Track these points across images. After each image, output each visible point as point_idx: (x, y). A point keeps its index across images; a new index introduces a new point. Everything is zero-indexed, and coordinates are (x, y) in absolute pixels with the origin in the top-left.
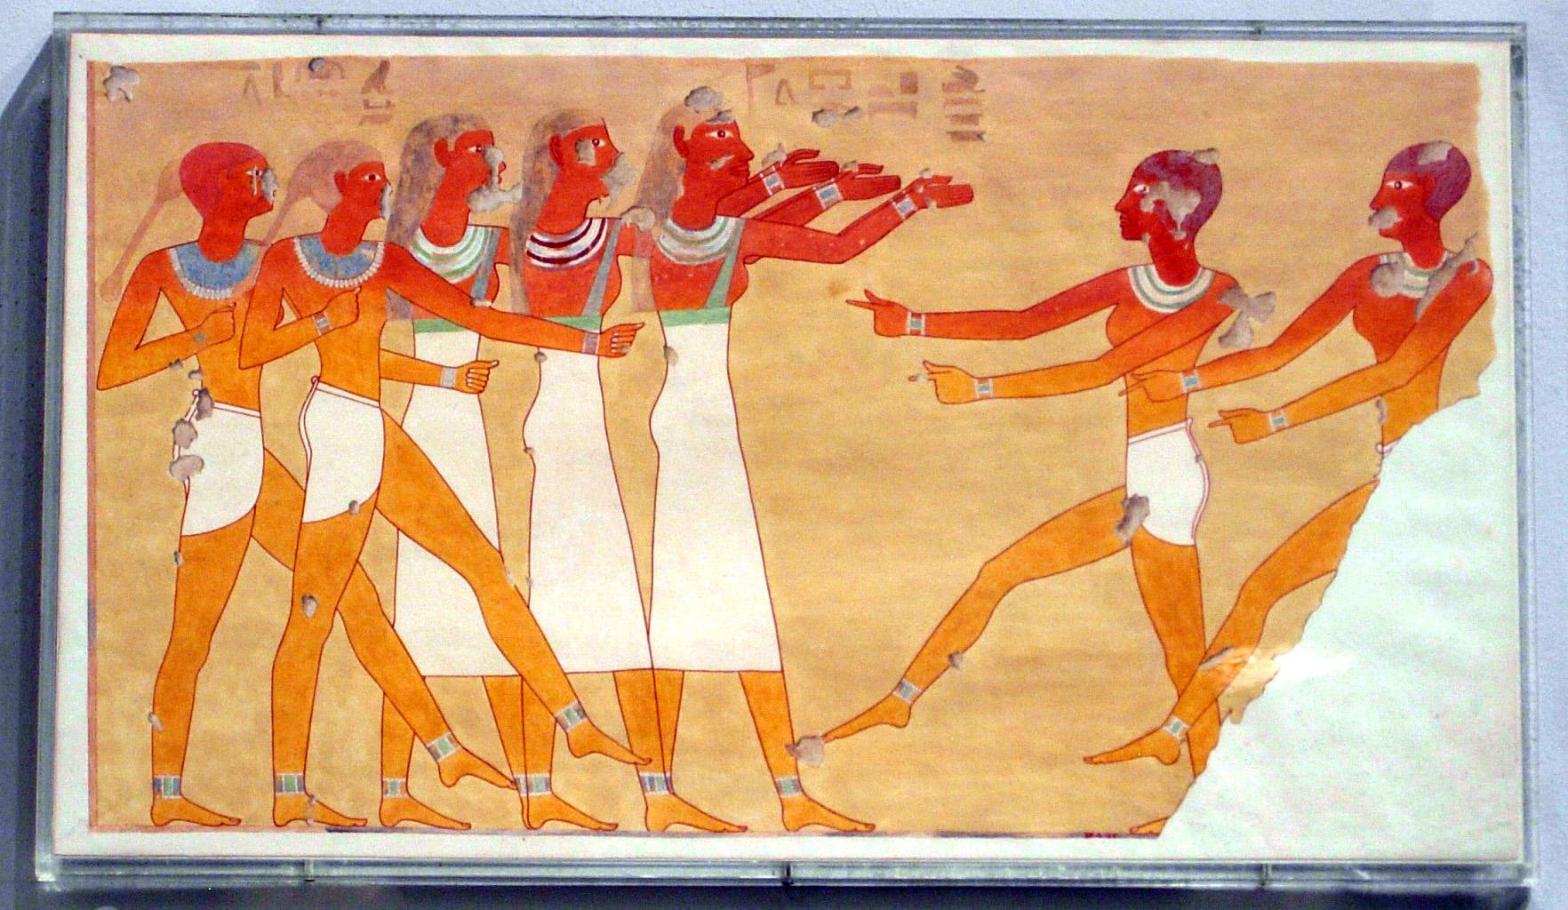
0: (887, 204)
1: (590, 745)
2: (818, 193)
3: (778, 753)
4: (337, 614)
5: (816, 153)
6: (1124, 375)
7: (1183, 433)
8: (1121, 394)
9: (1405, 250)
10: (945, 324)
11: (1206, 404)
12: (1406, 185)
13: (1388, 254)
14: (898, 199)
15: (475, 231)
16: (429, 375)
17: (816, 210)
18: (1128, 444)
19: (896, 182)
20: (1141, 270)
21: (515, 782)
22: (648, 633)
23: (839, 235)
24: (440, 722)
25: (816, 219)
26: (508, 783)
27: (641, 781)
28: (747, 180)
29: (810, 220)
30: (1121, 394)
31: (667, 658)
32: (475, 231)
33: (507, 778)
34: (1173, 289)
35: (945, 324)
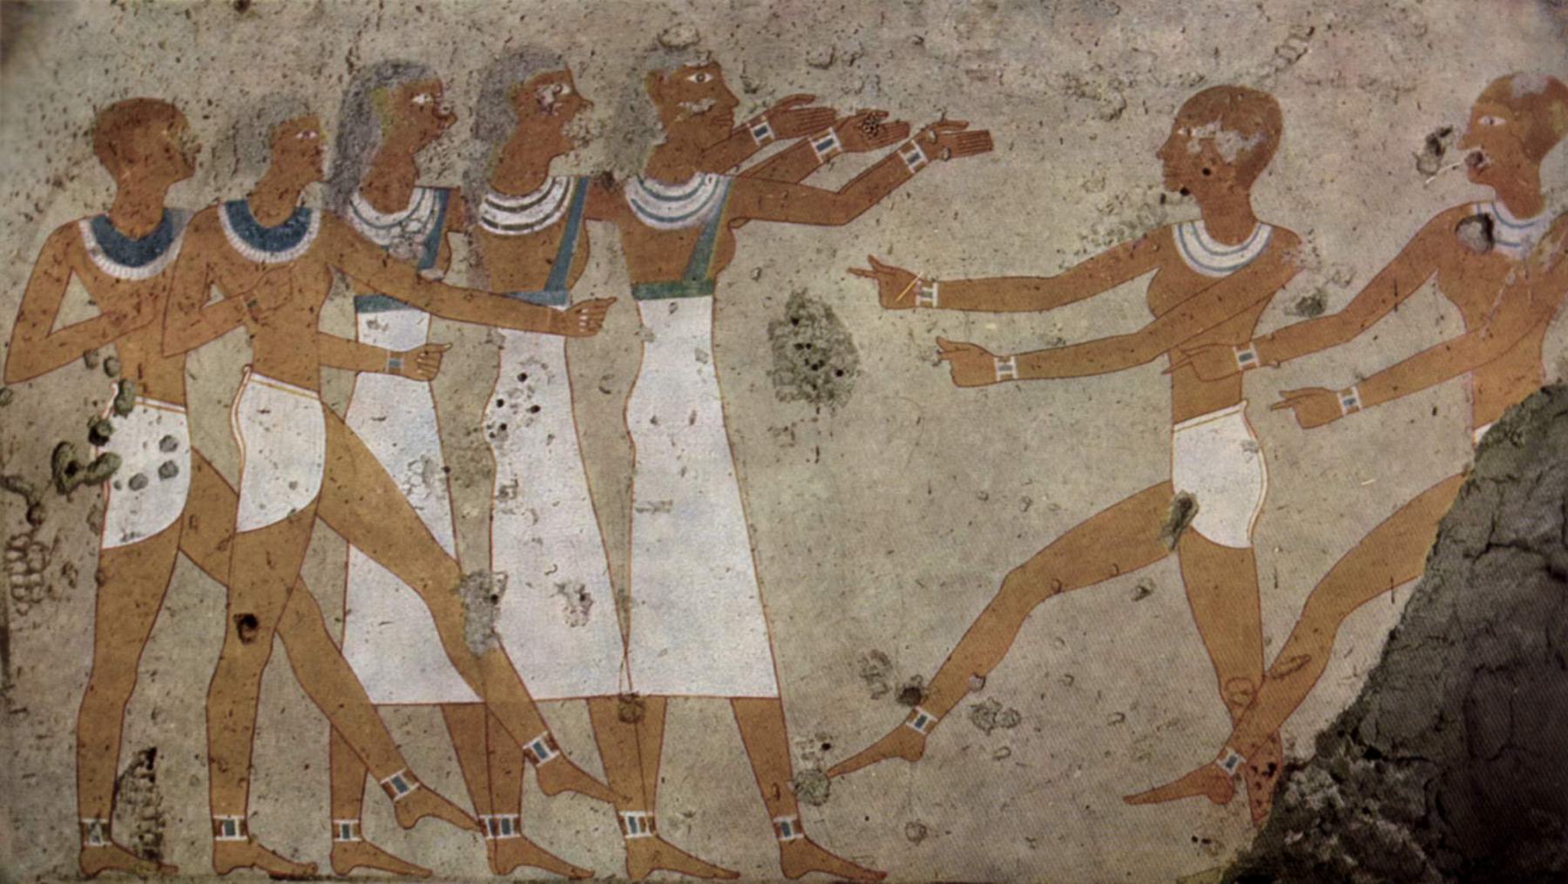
0: (892, 157)
1: (567, 779)
2: (814, 145)
3: (740, 466)
4: (277, 635)
5: (812, 99)
6: (1168, 351)
7: (1238, 419)
8: (1165, 372)
9: (1497, 198)
10: (960, 295)
11: (1262, 384)
12: (1499, 121)
13: (1478, 203)
14: (906, 148)
15: (423, 194)
16: (360, 359)
17: (808, 164)
18: (1173, 432)
19: (903, 128)
20: (1187, 229)
21: (481, 824)
22: (626, 642)
23: (839, 193)
24: (393, 754)
25: (466, 700)
26: (472, 825)
27: (621, 821)
28: (731, 131)
29: (471, 704)
30: (1165, 372)
31: (643, 689)
32: (423, 194)
33: (472, 819)
34: (1220, 248)
35: (960, 295)
